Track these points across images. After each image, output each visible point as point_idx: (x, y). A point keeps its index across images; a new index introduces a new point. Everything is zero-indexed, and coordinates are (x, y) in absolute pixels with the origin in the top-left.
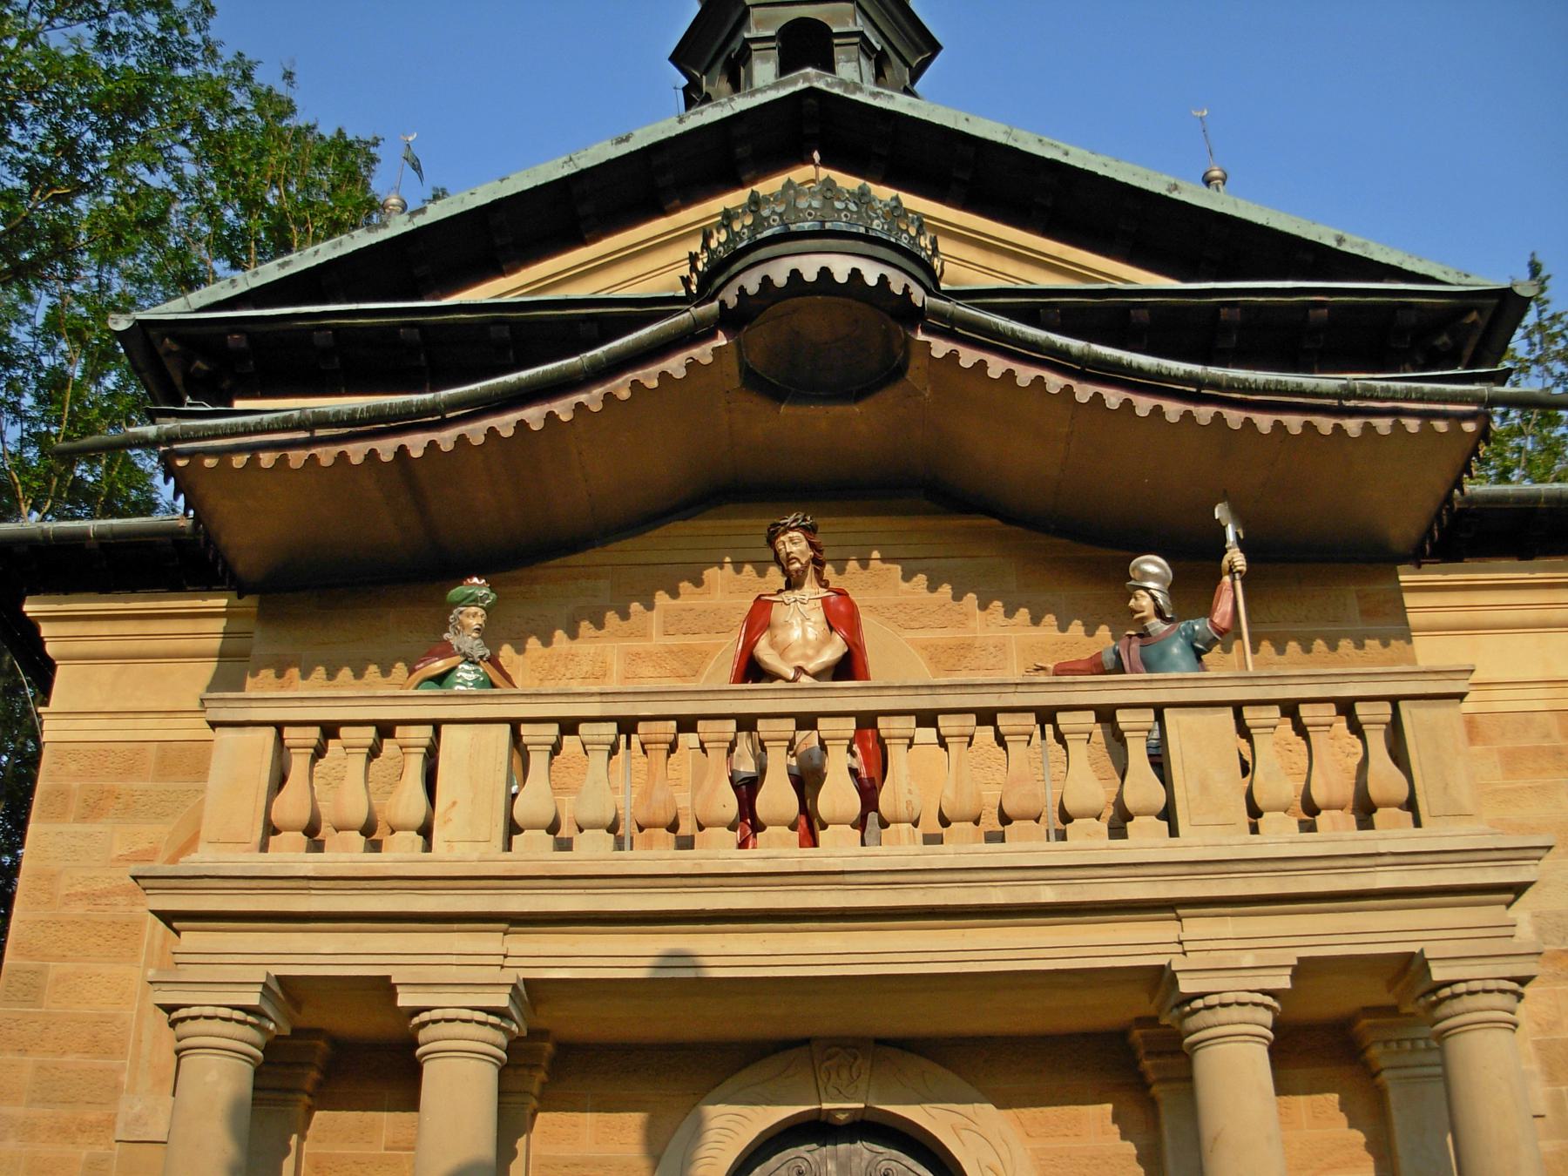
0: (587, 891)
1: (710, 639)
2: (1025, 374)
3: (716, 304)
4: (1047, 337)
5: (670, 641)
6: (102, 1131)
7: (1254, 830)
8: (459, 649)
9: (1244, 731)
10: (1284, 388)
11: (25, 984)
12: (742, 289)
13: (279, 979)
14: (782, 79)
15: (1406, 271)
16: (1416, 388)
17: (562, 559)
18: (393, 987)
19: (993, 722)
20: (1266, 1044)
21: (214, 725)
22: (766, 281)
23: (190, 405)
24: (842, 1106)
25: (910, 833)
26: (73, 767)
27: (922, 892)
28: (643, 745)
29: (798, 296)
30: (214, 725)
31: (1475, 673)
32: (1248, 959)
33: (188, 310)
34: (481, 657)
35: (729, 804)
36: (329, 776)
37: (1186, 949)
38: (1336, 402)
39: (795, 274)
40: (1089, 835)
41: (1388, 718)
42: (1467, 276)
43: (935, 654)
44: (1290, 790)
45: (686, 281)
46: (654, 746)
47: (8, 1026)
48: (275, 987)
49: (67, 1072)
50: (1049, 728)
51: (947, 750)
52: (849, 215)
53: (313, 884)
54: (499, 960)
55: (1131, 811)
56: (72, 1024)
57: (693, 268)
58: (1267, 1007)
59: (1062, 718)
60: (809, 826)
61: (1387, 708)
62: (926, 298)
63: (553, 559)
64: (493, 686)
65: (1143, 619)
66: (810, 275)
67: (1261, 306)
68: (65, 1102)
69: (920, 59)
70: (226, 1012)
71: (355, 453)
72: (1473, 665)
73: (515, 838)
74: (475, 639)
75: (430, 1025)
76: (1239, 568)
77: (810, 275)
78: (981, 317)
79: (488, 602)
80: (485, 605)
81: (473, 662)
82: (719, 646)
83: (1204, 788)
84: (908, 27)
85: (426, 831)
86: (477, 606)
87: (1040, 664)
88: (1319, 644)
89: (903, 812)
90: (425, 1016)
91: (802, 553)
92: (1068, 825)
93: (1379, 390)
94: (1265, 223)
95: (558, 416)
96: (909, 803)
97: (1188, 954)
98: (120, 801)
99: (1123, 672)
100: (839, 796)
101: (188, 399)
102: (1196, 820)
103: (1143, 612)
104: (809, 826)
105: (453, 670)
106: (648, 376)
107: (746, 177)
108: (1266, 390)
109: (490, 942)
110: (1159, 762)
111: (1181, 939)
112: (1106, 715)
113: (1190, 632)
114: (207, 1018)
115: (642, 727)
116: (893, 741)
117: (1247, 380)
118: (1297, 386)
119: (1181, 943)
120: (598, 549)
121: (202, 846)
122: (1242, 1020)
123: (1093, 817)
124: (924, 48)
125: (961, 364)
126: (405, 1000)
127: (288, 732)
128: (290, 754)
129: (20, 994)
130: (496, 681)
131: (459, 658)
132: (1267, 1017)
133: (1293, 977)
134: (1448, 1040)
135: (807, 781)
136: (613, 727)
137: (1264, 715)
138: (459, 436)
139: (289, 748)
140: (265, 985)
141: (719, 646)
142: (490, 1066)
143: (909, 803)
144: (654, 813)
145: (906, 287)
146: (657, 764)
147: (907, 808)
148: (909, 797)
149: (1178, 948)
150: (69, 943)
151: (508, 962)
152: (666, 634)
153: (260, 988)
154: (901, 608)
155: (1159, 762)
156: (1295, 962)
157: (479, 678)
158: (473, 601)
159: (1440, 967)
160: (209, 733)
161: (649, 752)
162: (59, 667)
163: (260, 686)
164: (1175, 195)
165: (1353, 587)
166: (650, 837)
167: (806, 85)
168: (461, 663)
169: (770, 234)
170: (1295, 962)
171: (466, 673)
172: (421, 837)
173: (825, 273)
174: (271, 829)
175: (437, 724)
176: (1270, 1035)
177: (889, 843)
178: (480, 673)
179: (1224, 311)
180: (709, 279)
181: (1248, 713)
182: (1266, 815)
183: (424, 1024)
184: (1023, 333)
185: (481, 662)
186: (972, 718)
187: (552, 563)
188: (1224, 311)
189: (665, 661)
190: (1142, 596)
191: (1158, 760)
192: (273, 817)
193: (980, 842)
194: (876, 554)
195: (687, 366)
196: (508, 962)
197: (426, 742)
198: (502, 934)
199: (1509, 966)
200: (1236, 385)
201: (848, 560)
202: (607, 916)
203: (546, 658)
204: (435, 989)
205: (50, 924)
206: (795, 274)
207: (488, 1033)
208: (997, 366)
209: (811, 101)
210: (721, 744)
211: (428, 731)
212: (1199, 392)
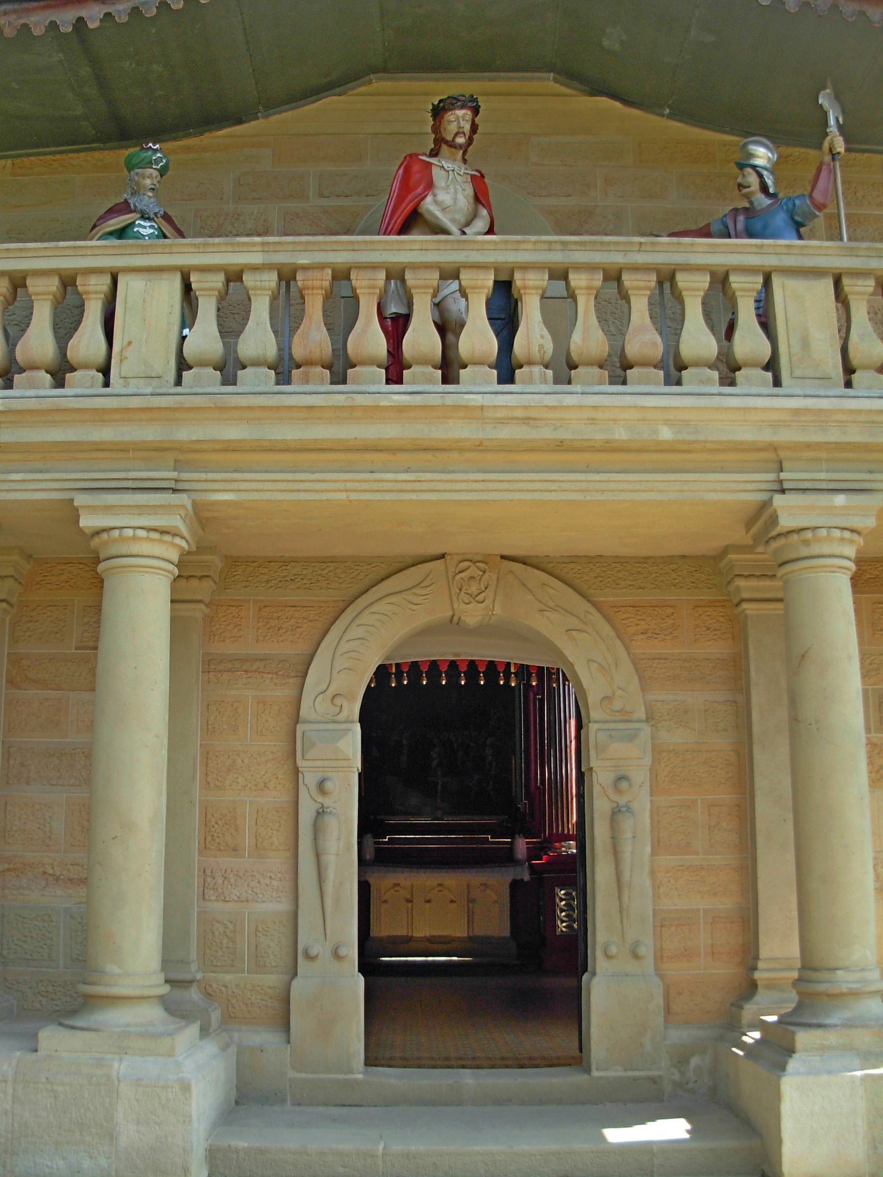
5: (325, 202)
7: (848, 384)
8: (135, 206)
19: (565, 278)
25: (541, 375)
34: (156, 214)
36: (23, 324)
54: (172, 485)
64: (165, 237)
65: (752, 193)
71: (36, 24)
73: (184, 373)
79: (161, 164)
80: (159, 167)
83: (805, 344)
85: (106, 371)
86: (152, 168)
96: (541, 346)
99: (729, 236)
102: (797, 372)
103: (749, 187)
105: (132, 224)
110: (766, 322)
113: (791, 206)
123: (705, 365)
126: (87, 522)
130: (168, 234)
143: (541, 346)
144: (310, 352)
146: (313, 307)
147: (539, 351)
148: (542, 341)
152: (321, 196)
155: (766, 322)
157: (153, 233)
158: (147, 163)
166: (307, 374)
169: (661, 1123)
171: (146, 229)
177: (523, 382)
178: (155, 229)
185: (155, 219)
189: (320, 220)
190: (749, 173)
191: (763, 319)
192: (185, 355)
193: (604, 384)
203: (214, 217)
211: (107, 280)
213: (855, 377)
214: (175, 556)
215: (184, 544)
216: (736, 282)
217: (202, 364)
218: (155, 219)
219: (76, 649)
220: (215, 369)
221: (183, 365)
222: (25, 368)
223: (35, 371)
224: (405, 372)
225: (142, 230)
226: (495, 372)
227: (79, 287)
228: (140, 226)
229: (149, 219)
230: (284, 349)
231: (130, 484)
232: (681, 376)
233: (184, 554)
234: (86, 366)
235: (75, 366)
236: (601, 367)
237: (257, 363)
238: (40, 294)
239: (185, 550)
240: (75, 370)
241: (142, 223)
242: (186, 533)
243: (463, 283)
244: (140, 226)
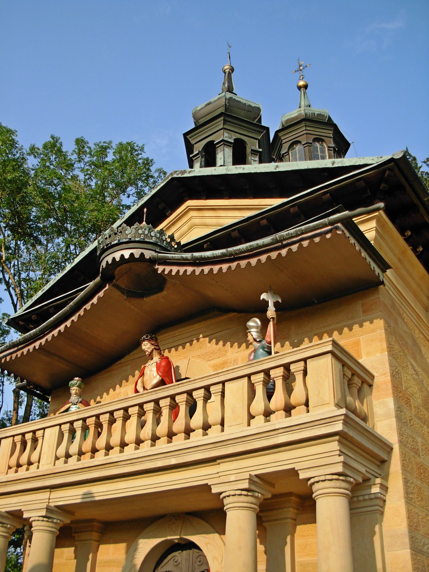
0: (62, 476)
4: (181, 256)
10: (253, 247)
13: (256, 476)
15: (357, 166)
16: (299, 229)
17: (119, 361)
18: (210, 486)
27: (139, 465)
29: (118, 267)
32: (233, 478)
38: (280, 244)
40: (196, 436)
42: (381, 157)
43: (216, 367)
48: (256, 479)
52: (119, 237)
53: (7, 483)
63: (116, 362)
66: (127, 256)
67: (306, 202)
69: (262, 135)
70: (330, 477)
74: (75, 397)
75: (315, 484)
76: (271, 317)
77: (127, 256)
78: (164, 256)
81: (75, 404)
84: (251, 127)
88: (346, 330)
90: (312, 481)
91: (148, 348)
93: (285, 235)
94: (307, 168)
105: (69, 408)
106: (88, 306)
107: (168, 214)
108: (247, 251)
109: (44, 495)
114: (322, 481)
117: (240, 249)
118: (257, 245)
120: (128, 356)
122: (234, 502)
124: (263, 131)
131: (71, 404)
137: (257, 377)
140: (250, 479)
151: (220, 474)
153: (248, 481)
154: (207, 354)
159: (302, 473)
164: (278, 170)
165: (360, 302)
168: (71, 405)
173: (132, 255)
174: (251, 417)
179: (291, 210)
183: (313, 484)
184: (175, 257)
187: (116, 363)
188: (291, 210)
194: (201, 336)
197: (221, 390)
199: (330, 469)
200: (237, 252)
201: (193, 340)
202: (130, 474)
204: (32, 511)
207: (243, 498)
209: (175, 182)
212: (234, 257)
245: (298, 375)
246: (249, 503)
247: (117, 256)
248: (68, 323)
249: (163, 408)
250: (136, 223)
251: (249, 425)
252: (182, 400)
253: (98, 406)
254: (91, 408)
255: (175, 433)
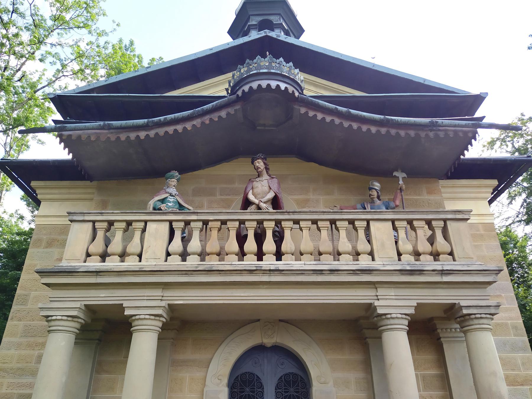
1: (233, 197)
2: (328, 119)
3: (235, 95)
6: (43, 345)
9: (395, 229)
11: (23, 299)
12: (243, 91)
14: (259, 33)
19: (317, 224)
20: (406, 332)
21: (71, 221)
22: (251, 88)
23: (68, 120)
24: (268, 342)
26: (45, 232)
28: (210, 228)
30: (71, 221)
31: (472, 212)
33: (74, 93)
34: (175, 194)
35: (235, 247)
37: (379, 298)
39: (260, 86)
41: (443, 226)
44: (409, 247)
45: (227, 90)
46: (213, 229)
47: (16, 312)
49: (33, 327)
50: (333, 226)
51: (302, 231)
54: (160, 298)
55: (360, 252)
56: (37, 311)
57: (230, 85)
58: (406, 319)
59: (338, 223)
60: (260, 255)
61: (442, 223)
62: (299, 95)
68: (32, 336)
72: (472, 210)
82: (237, 199)
85: (140, 256)
87: (336, 205)
89: (289, 251)
92: (340, 256)
95: (187, 128)
97: (379, 300)
98: (59, 242)
100: (269, 245)
101: (68, 118)
104: (260, 255)
109: (158, 292)
111: (377, 295)
112: (351, 222)
115: (210, 223)
116: (286, 229)
119: (377, 296)
121: (63, 261)
125: (309, 115)
126: (127, 312)
127: (97, 224)
128: (97, 231)
129: (21, 302)
132: (406, 322)
133: (415, 310)
134: (468, 333)
135: (260, 238)
136: (201, 223)
138: (156, 133)
139: (97, 229)
141: (237, 199)
142: (155, 333)
145: (293, 91)
147: (290, 249)
149: (376, 298)
150: (38, 286)
151: (164, 298)
156: (416, 305)
160: (70, 223)
161: (212, 231)
162: (42, 202)
163: (96, 208)
167: (265, 34)
170: (416, 305)
172: (138, 257)
173: (269, 85)
174: (88, 255)
175: (146, 222)
176: (407, 328)
180: (233, 90)
181: (396, 223)
182: (403, 256)
186: (310, 223)
192: (89, 251)
195: (227, 114)
196: (164, 298)
197: (142, 227)
198: (162, 289)
204: (156, 308)
205: (32, 280)
206: (260, 86)
208: (320, 116)
210: (234, 229)
213: (402, 257)
214: (160, 324)
215: (164, 320)
216: (359, 227)
217: (175, 254)
218: (175, 196)
219: (124, 358)
220: (236, 255)
221: (168, 254)
222: (190, 254)
223: (114, 256)
224: (107, 258)
225: (170, 199)
226: (256, 257)
227: (283, 225)
228: (169, 198)
229: (173, 196)
230: (204, 247)
231: (145, 298)
232: (358, 257)
233: (164, 324)
234: (133, 254)
235: (91, 255)
236: (311, 255)
237: (194, 254)
238: (286, 228)
239: (165, 322)
240: (91, 256)
241: (170, 197)
242: (165, 315)
243: (301, 226)
244: (169, 198)
245: (100, 231)
246: (72, 327)
247: (264, 83)
248: (179, 128)
249: (97, 230)
250: (238, 66)
251: (166, 261)
252: (216, 226)
253: (243, 212)
254: (246, 212)
255: (128, 254)
